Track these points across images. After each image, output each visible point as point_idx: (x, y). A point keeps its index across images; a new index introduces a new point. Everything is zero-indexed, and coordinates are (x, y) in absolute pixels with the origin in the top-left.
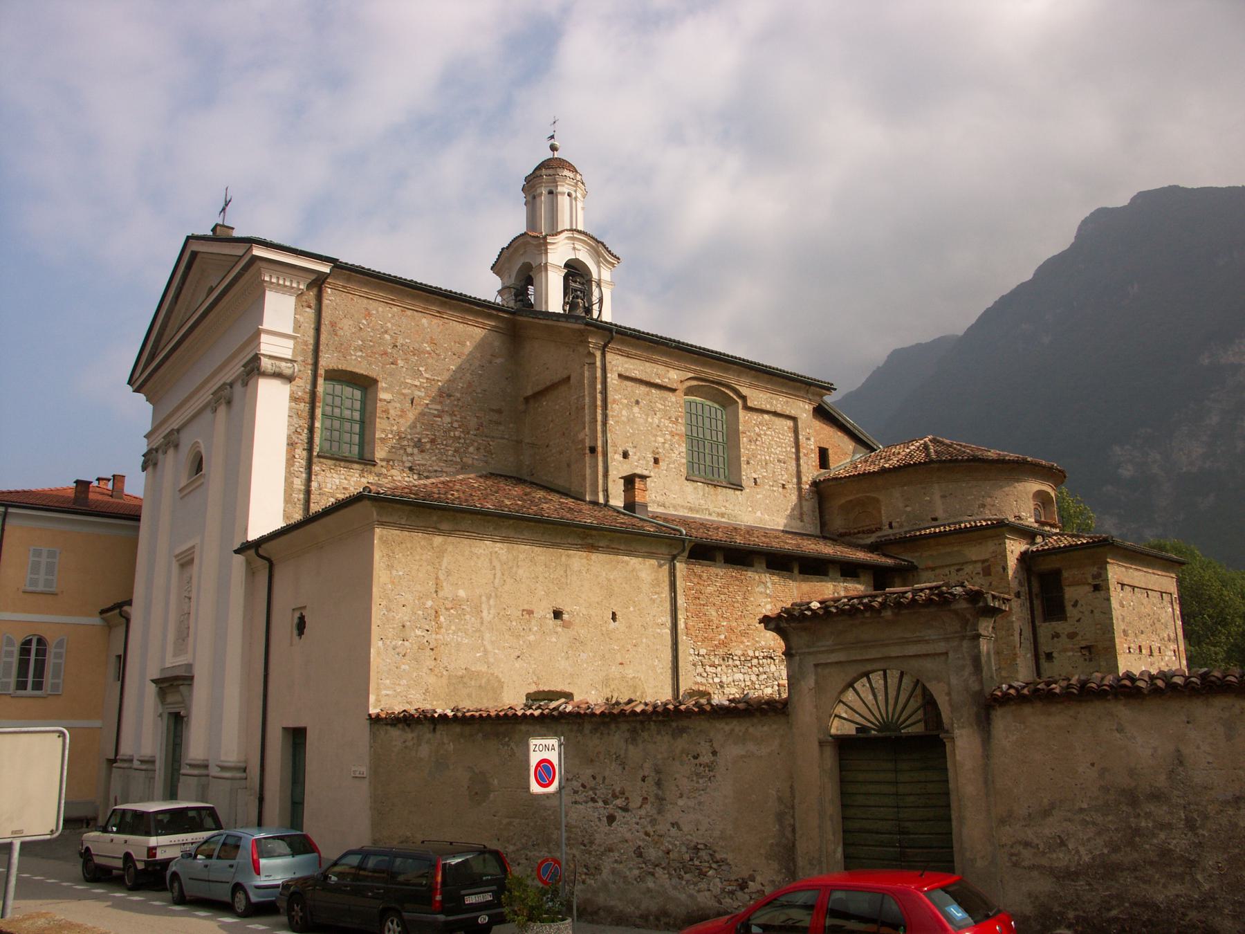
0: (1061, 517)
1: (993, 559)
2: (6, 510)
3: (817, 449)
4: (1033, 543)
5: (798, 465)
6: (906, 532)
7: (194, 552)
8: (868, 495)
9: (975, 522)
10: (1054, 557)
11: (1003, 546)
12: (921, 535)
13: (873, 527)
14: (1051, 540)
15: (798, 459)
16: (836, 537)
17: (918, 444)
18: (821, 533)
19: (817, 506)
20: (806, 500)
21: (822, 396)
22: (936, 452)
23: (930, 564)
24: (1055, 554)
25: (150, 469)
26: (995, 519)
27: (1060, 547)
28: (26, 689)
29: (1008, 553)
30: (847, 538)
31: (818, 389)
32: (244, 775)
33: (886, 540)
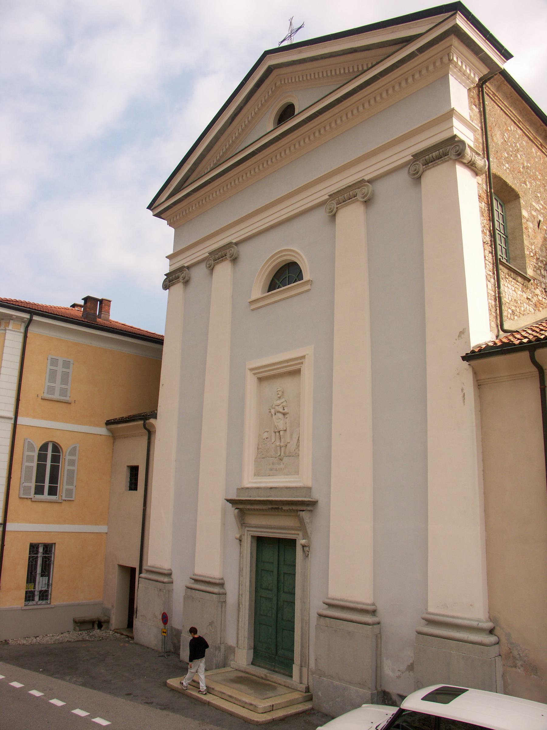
2: (31, 317)
7: (302, 363)
25: (178, 288)
28: (43, 494)
32: (492, 639)
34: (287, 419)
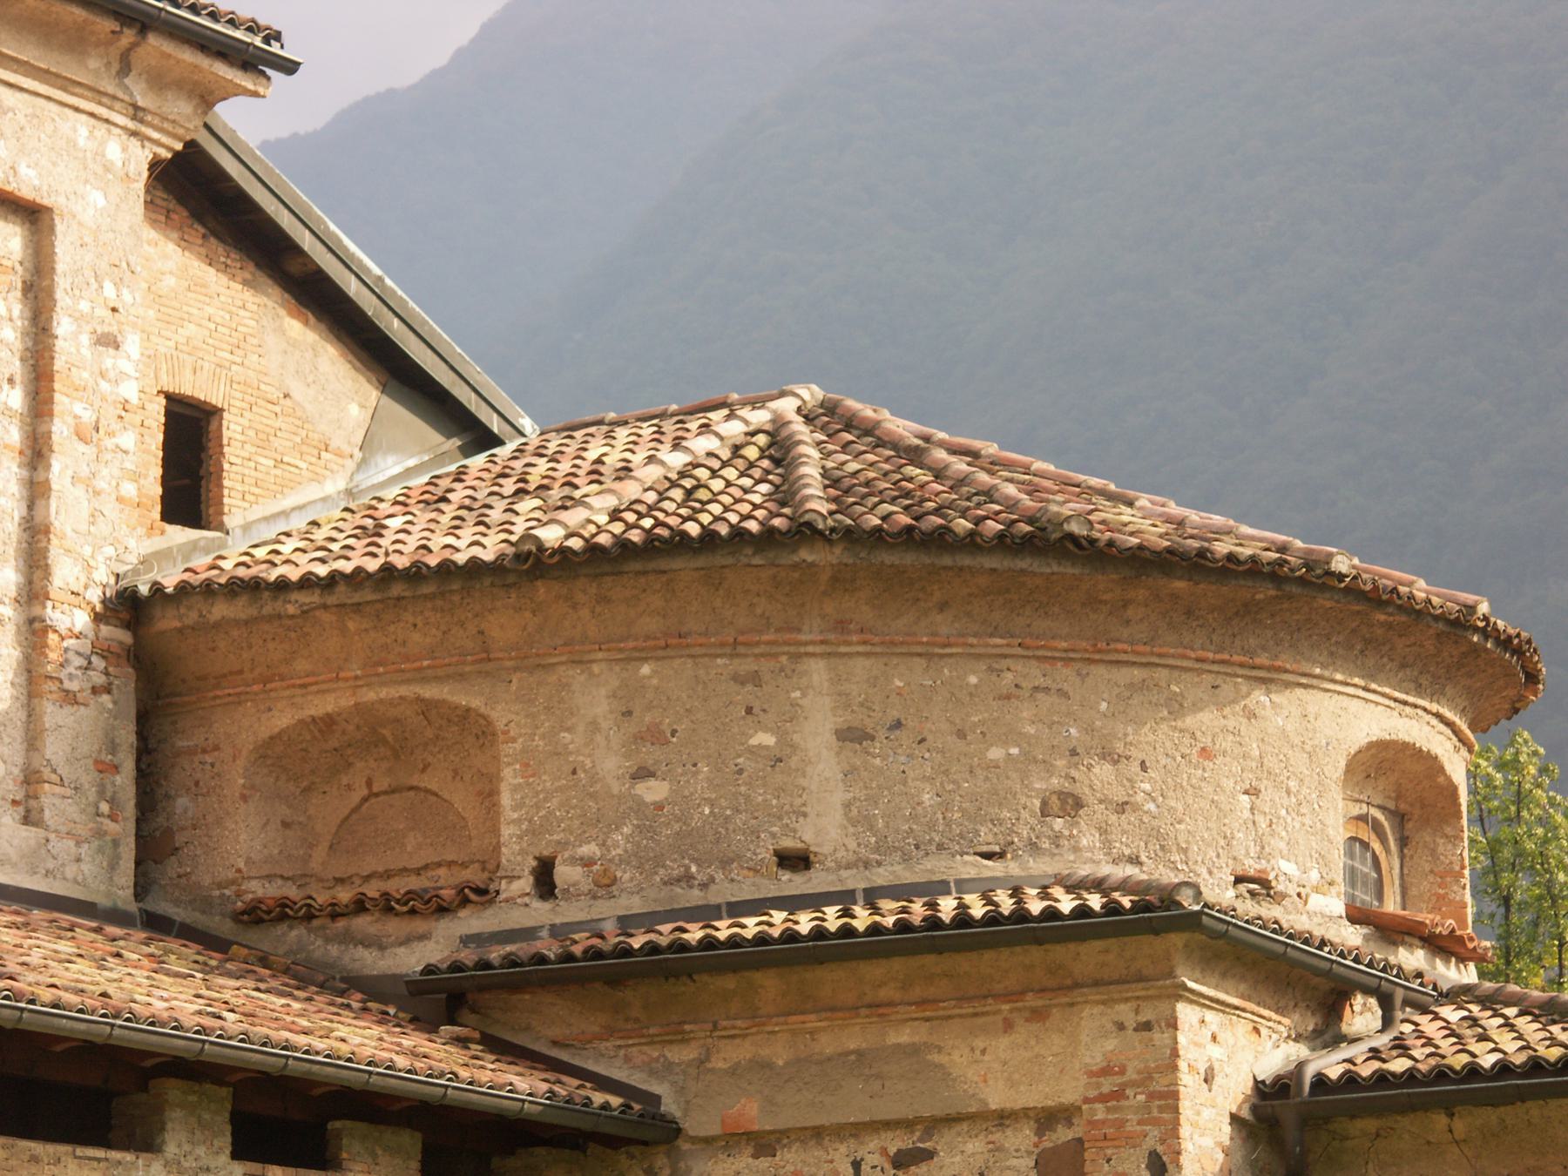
0: (1490, 883)
1: (1100, 1112)
3: (157, 408)
4: (1328, 1034)
5: (36, 491)
6: (627, 923)
8: (429, 692)
9: (1016, 892)
10: (1441, 1120)
11: (1159, 1037)
12: (709, 943)
13: (445, 882)
14: (1430, 1027)
15: (36, 452)
16: (223, 927)
17: (734, 429)
18: (141, 891)
19: (127, 736)
20: (70, 698)
21: (206, 98)
22: (831, 480)
23: (751, 1112)
24: (1448, 1105)
26: (1125, 886)
27: (1473, 1071)
29: (1188, 1082)
30: (295, 934)
31: (188, 56)
33: (511, 961)
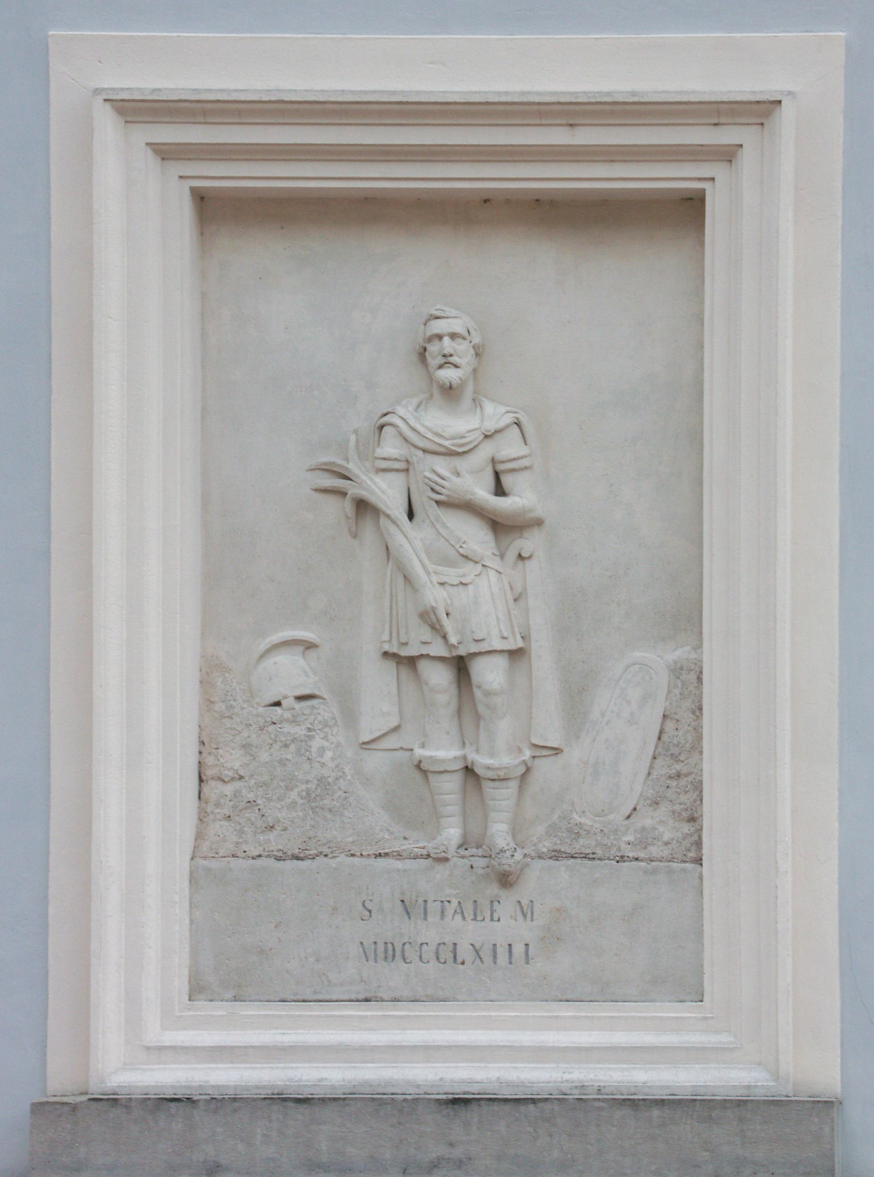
34: (532, 566)
